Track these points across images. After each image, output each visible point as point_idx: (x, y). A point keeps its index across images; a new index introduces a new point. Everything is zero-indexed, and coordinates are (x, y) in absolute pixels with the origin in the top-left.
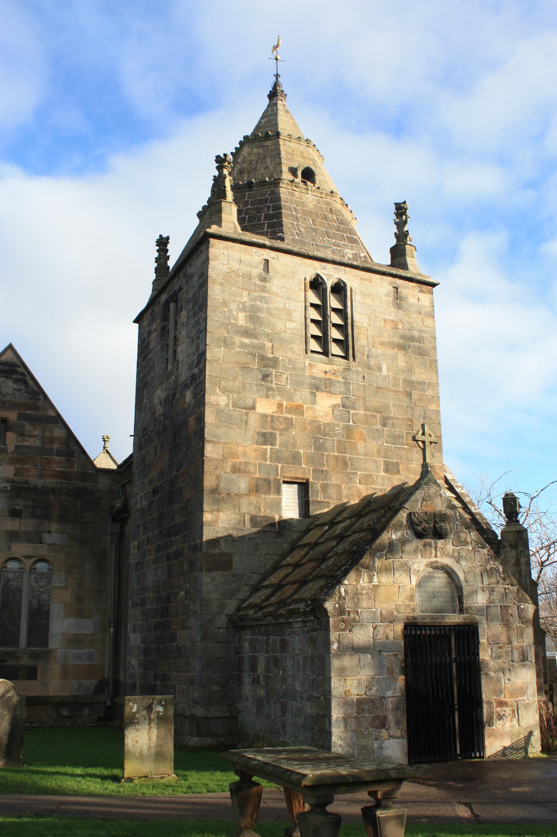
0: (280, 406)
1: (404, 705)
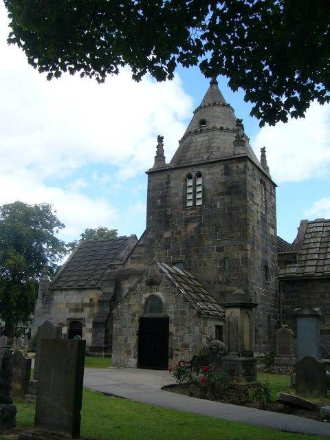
0: (173, 233)
1: (137, 347)
